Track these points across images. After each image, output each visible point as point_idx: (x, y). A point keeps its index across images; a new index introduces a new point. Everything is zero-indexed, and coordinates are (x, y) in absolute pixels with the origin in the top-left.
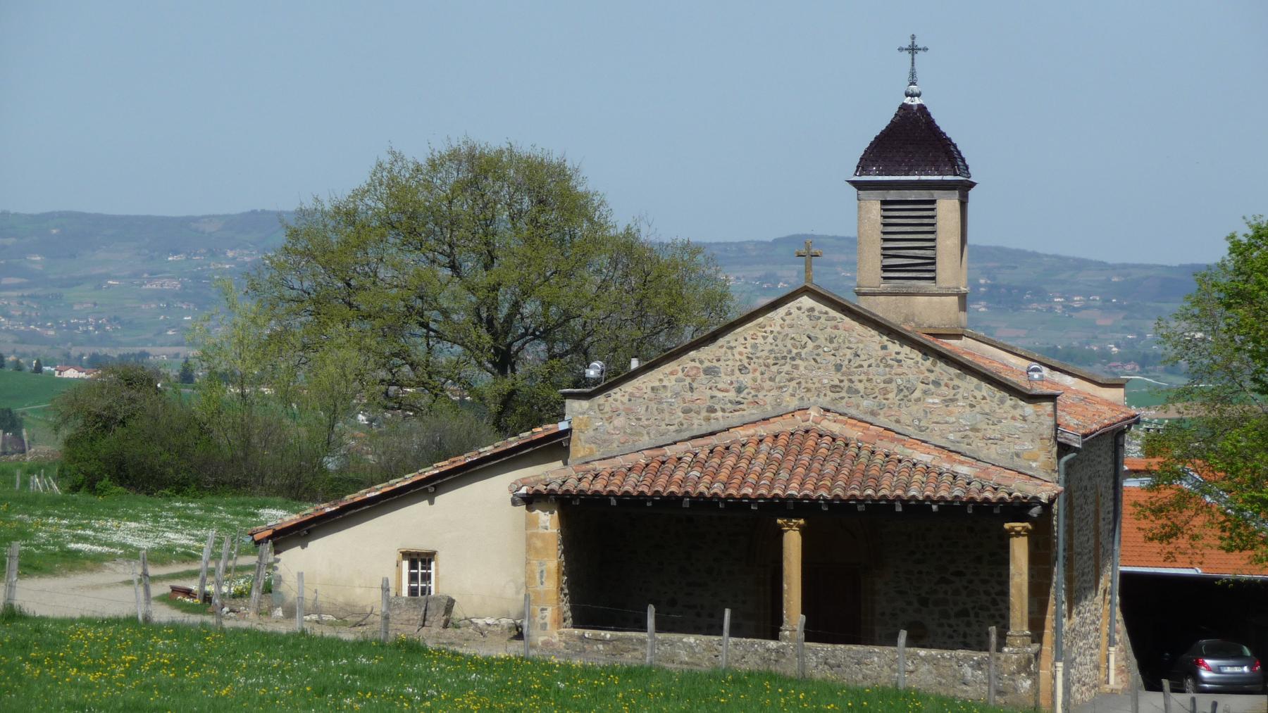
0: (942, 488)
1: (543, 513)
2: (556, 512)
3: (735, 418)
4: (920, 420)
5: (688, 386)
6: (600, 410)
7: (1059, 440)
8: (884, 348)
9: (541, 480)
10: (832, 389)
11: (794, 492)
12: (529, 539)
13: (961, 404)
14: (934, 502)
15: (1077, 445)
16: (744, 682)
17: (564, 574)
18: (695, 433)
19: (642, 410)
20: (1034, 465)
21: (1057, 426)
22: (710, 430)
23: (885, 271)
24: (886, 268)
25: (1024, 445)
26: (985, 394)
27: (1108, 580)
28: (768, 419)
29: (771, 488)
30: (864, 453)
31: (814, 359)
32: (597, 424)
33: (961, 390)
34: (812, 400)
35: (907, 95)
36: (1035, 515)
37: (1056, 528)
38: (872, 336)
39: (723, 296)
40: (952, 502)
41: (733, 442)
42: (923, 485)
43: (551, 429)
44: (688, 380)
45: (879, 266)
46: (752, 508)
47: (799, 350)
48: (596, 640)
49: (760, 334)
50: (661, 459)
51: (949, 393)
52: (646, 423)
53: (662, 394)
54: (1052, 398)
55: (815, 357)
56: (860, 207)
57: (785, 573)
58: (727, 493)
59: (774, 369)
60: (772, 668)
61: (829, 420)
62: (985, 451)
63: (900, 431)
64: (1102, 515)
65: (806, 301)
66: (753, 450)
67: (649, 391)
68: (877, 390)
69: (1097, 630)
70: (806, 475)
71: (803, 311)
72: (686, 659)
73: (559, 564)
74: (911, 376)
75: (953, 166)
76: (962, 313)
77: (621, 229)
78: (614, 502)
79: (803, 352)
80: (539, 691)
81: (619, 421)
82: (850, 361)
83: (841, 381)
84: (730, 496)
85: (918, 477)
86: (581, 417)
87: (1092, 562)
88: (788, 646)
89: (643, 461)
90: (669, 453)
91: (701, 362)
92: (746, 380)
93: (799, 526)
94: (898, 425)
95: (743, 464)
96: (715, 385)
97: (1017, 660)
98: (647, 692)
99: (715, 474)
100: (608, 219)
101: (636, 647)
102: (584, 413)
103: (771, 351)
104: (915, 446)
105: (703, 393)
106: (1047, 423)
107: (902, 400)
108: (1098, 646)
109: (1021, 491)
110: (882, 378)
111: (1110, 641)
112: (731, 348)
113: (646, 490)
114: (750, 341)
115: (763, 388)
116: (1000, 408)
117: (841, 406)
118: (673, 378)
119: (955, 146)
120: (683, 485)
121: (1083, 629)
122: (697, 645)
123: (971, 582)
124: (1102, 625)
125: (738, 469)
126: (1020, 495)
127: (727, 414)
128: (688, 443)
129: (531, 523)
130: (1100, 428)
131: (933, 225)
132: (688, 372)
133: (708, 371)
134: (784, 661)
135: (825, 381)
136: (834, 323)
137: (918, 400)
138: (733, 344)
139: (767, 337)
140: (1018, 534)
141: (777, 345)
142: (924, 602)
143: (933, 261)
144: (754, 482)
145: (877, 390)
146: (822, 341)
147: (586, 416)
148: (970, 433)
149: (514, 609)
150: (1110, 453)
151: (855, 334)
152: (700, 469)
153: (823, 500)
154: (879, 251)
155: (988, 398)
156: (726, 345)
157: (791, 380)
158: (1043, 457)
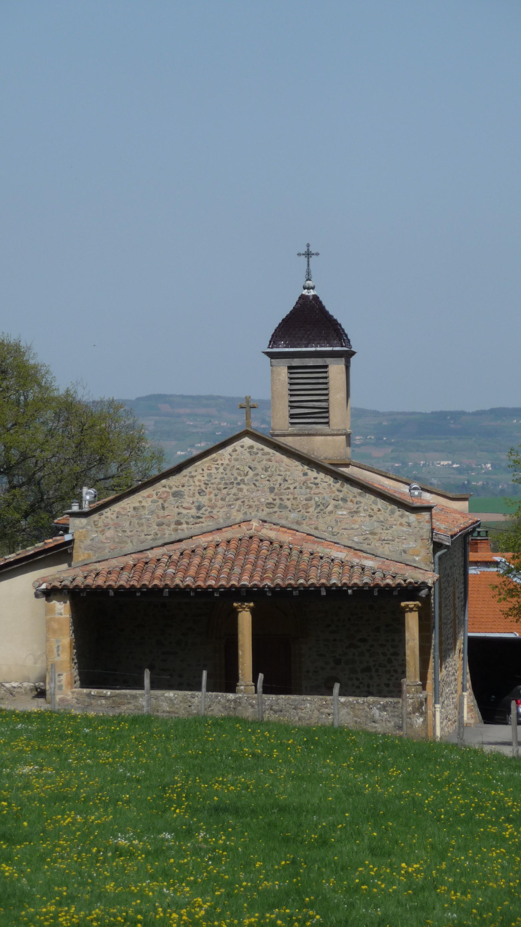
0: (355, 577)
1: (59, 603)
2: (68, 602)
3: (196, 529)
4: (332, 528)
5: (161, 506)
6: (95, 525)
7: (434, 540)
8: (305, 474)
9: (57, 578)
10: (268, 506)
11: (246, 583)
12: (48, 623)
13: (362, 515)
14: (349, 588)
15: (448, 544)
16: (221, 725)
17: (74, 648)
18: (167, 540)
19: (126, 524)
20: (417, 559)
21: (433, 529)
22: (178, 538)
23: (291, 418)
24: (292, 416)
25: (409, 544)
26: (380, 508)
27: (461, 644)
28: (221, 529)
29: (229, 580)
30: (295, 552)
31: (254, 484)
32: (93, 536)
33: (362, 505)
34: (253, 514)
35: (305, 288)
36: (424, 596)
37: (433, 605)
38: (296, 466)
39: (141, 439)
40: (363, 587)
41: (197, 547)
42: (341, 575)
43: (58, 540)
44: (161, 501)
45: (287, 414)
46: (215, 595)
47: (243, 477)
48: (100, 696)
49: (213, 466)
50: (145, 560)
51: (354, 507)
52: (130, 534)
53: (142, 512)
54: (429, 509)
55: (255, 482)
56: (272, 371)
57: (240, 643)
58: (197, 584)
59: (225, 491)
60: (231, 713)
61: (267, 529)
62: (381, 550)
63: (319, 536)
64: (457, 595)
65: (247, 441)
66: (212, 552)
67: (132, 510)
68: (300, 506)
69: (455, 680)
70: (254, 570)
71: (245, 448)
72: (168, 709)
73: (71, 640)
74: (325, 495)
75: (340, 340)
76: (348, 448)
77: (62, 391)
78: (112, 593)
79: (246, 479)
80: (72, 736)
81: (109, 533)
82: (280, 485)
83: (274, 500)
84: (199, 587)
85: (336, 569)
86: (81, 530)
87: (452, 630)
88: (243, 697)
89: (131, 563)
90: (150, 556)
91: (170, 488)
92: (204, 500)
93: (250, 608)
94: (316, 531)
95: (206, 563)
96: (181, 504)
97: (413, 703)
98: (152, 733)
99: (186, 570)
100: (53, 384)
101: (129, 701)
102: (83, 528)
103: (222, 479)
104: (330, 547)
105: (172, 511)
106: (427, 528)
107: (319, 512)
108: (456, 692)
109: (413, 578)
110: (305, 497)
111: (463, 688)
112: (192, 477)
113: (135, 583)
114: (206, 472)
115: (216, 506)
116: (391, 517)
117: (275, 518)
118: (149, 500)
119: (340, 325)
120: (163, 579)
121: (448, 679)
122: (176, 698)
123: (372, 646)
124: (458, 677)
125: (202, 567)
126: (412, 581)
127: (190, 526)
128: (164, 548)
129: (49, 611)
130: (460, 531)
131: (326, 383)
132: (161, 495)
133: (176, 494)
134: (240, 708)
135: (263, 500)
136: (268, 457)
137: (331, 512)
138: (194, 474)
139: (219, 468)
140: (411, 610)
141: (226, 474)
142: (338, 662)
143: (326, 410)
144: (216, 576)
145: (300, 506)
146: (259, 470)
147: (85, 530)
148: (370, 536)
149: (34, 675)
150: (461, 549)
151: (283, 465)
152: (174, 567)
153: (267, 588)
154: (287, 404)
155: (382, 510)
156: (188, 475)
157: (237, 499)
158: (423, 552)
